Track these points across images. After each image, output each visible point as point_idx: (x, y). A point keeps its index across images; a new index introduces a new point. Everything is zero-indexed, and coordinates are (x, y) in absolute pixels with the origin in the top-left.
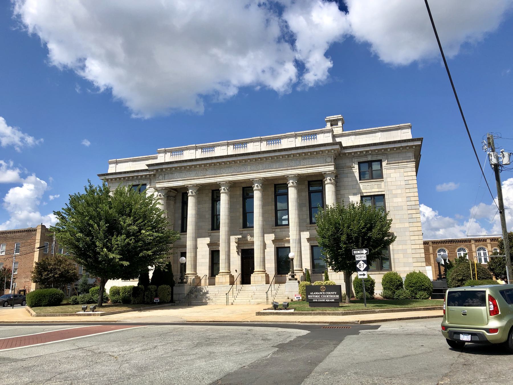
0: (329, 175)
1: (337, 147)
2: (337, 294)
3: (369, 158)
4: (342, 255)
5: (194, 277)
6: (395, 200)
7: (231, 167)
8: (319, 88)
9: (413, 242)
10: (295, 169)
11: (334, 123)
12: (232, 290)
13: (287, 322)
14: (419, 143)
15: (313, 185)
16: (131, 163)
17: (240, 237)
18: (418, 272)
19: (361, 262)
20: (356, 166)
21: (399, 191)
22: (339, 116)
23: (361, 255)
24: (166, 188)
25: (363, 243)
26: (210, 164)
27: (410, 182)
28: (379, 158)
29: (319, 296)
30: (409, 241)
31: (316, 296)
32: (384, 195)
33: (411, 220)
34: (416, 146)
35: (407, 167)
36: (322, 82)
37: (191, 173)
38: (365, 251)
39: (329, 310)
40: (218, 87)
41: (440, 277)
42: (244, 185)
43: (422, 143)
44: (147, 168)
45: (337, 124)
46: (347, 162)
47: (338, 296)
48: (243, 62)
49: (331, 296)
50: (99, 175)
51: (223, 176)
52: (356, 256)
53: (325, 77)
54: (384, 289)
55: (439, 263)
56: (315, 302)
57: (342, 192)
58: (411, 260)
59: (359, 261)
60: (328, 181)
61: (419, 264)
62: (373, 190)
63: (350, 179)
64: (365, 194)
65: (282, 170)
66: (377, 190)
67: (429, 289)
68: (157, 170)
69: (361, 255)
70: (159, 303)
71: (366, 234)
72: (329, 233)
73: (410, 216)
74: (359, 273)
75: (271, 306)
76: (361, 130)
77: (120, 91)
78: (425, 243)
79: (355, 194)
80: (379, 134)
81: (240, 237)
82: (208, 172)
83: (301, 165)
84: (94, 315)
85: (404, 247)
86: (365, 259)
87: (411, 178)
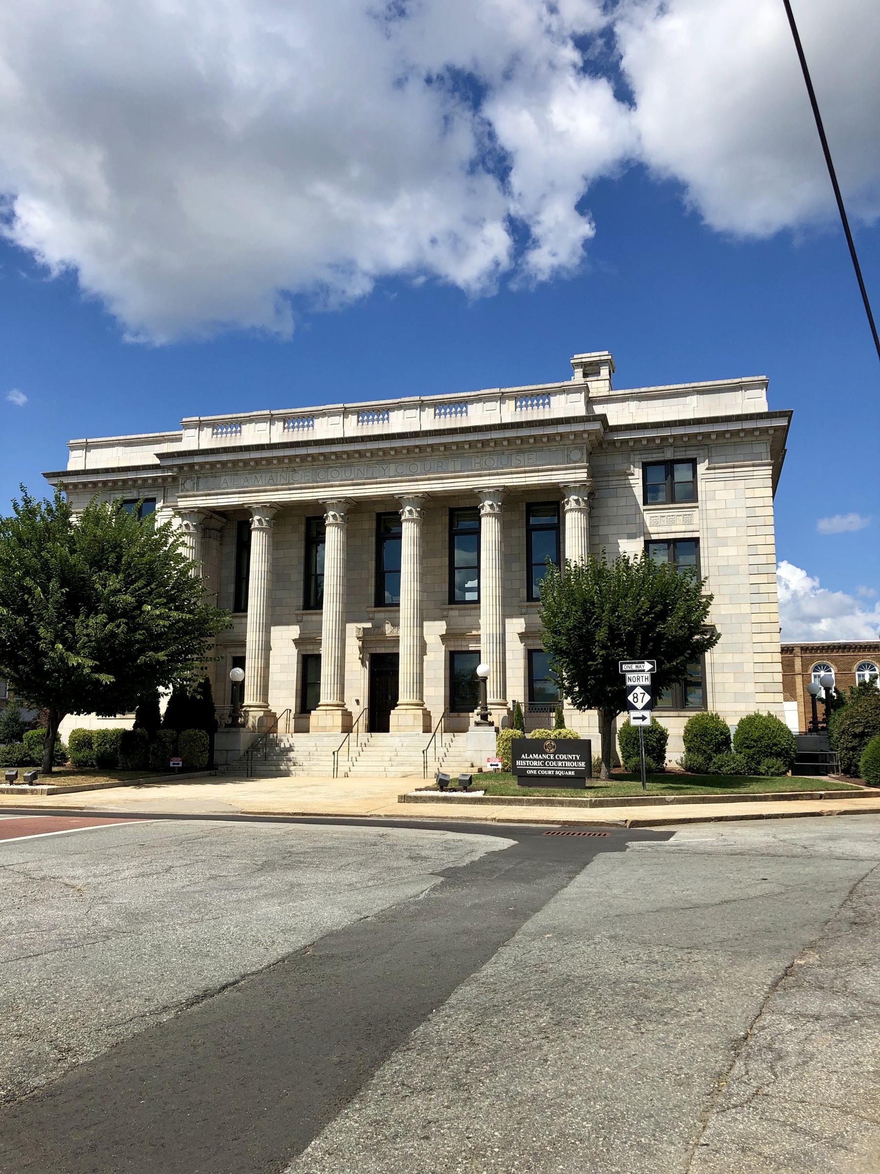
0: (575, 491)
1: (597, 426)
2: (581, 760)
3: (669, 455)
4: (596, 672)
5: (262, 714)
6: (722, 551)
7: (350, 465)
8: (560, 285)
9: (758, 648)
10: (498, 474)
11: (591, 369)
12: (346, 743)
13: (468, 818)
14: (783, 422)
15: (535, 514)
16: (120, 449)
17: (369, 625)
18: (765, 714)
19: (639, 690)
20: (638, 472)
21: (732, 532)
22: (604, 355)
23: (639, 675)
24: (201, 510)
25: (643, 648)
26: (303, 458)
27: (759, 511)
28: (691, 454)
29: (540, 763)
30: (749, 646)
31: (535, 763)
32: (696, 540)
33: (756, 599)
34: (776, 429)
35: (752, 477)
36: (568, 271)
37: (258, 476)
38: (647, 666)
39: (562, 794)
40: (326, 276)
41: (814, 726)
42: (381, 509)
43: (789, 422)
44: (157, 461)
45: (598, 373)
46: (616, 461)
47: (583, 764)
48: (385, 218)
49: (568, 764)
50: (47, 475)
51: (332, 486)
52: (628, 675)
53: (576, 261)
54: (689, 750)
55: (813, 696)
56: (532, 776)
57: (603, 530)
58: (750, 688)
59: (634, 687)
60: (573, 504)
61: (769, 697)
62: (674, 528)
63: (623, 502)
64: (654, 537)
65: (468, 477)
66: (683, 528)
67: (787, 752)
68: (180, 467)
69: (639, 675)
70: (182, 770)
71: (652, 626)
72: (570, 624)
73: (754, 589)
74: (633, 714)
75: (433, 782)
76: (652, 389)
77: (96, 276)
78: (786, 650)
79: (632, 536)
80: (693, 399)
81: (369, 625)
82: (297, 477)
83: (511, 467)
84: (33, 792)
85: (738, 658)
86: (648, 683)
87: (760, 502)
